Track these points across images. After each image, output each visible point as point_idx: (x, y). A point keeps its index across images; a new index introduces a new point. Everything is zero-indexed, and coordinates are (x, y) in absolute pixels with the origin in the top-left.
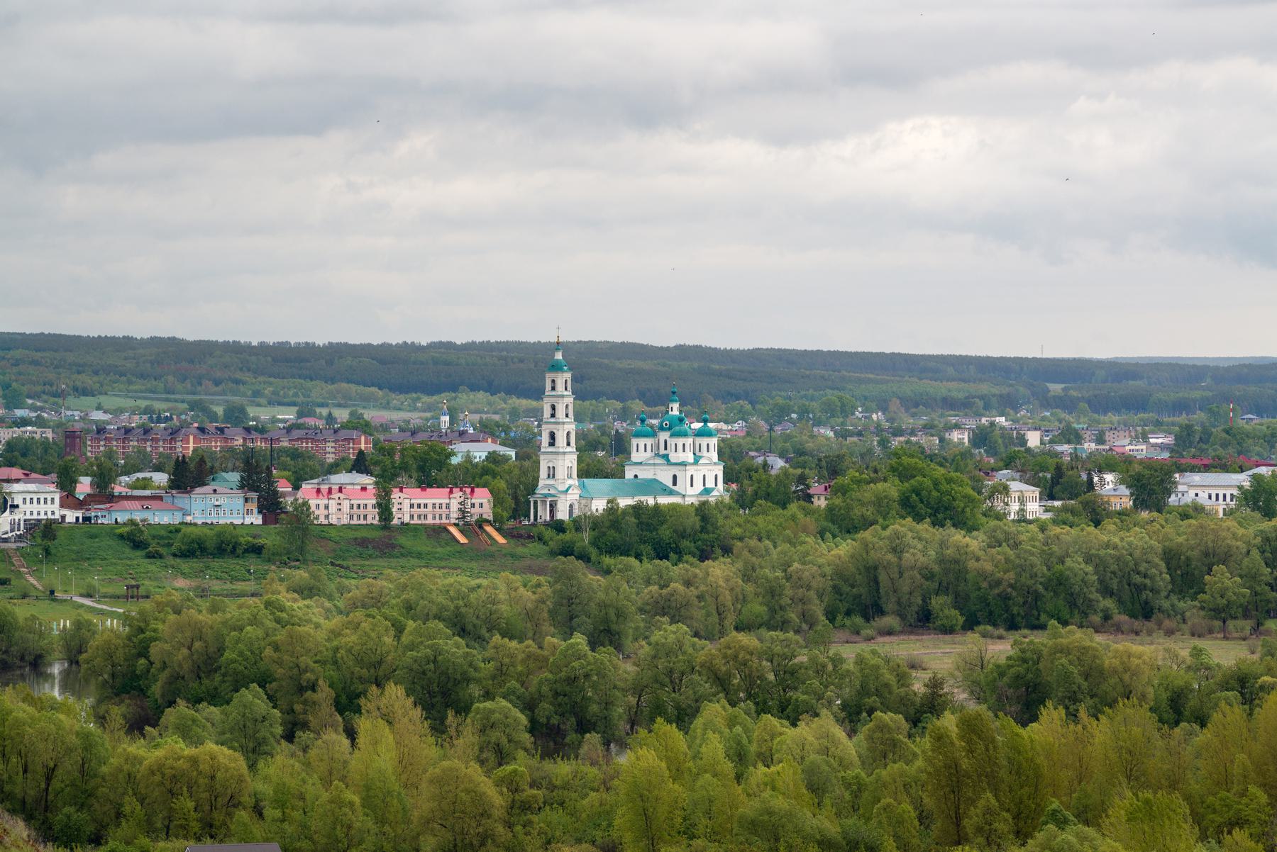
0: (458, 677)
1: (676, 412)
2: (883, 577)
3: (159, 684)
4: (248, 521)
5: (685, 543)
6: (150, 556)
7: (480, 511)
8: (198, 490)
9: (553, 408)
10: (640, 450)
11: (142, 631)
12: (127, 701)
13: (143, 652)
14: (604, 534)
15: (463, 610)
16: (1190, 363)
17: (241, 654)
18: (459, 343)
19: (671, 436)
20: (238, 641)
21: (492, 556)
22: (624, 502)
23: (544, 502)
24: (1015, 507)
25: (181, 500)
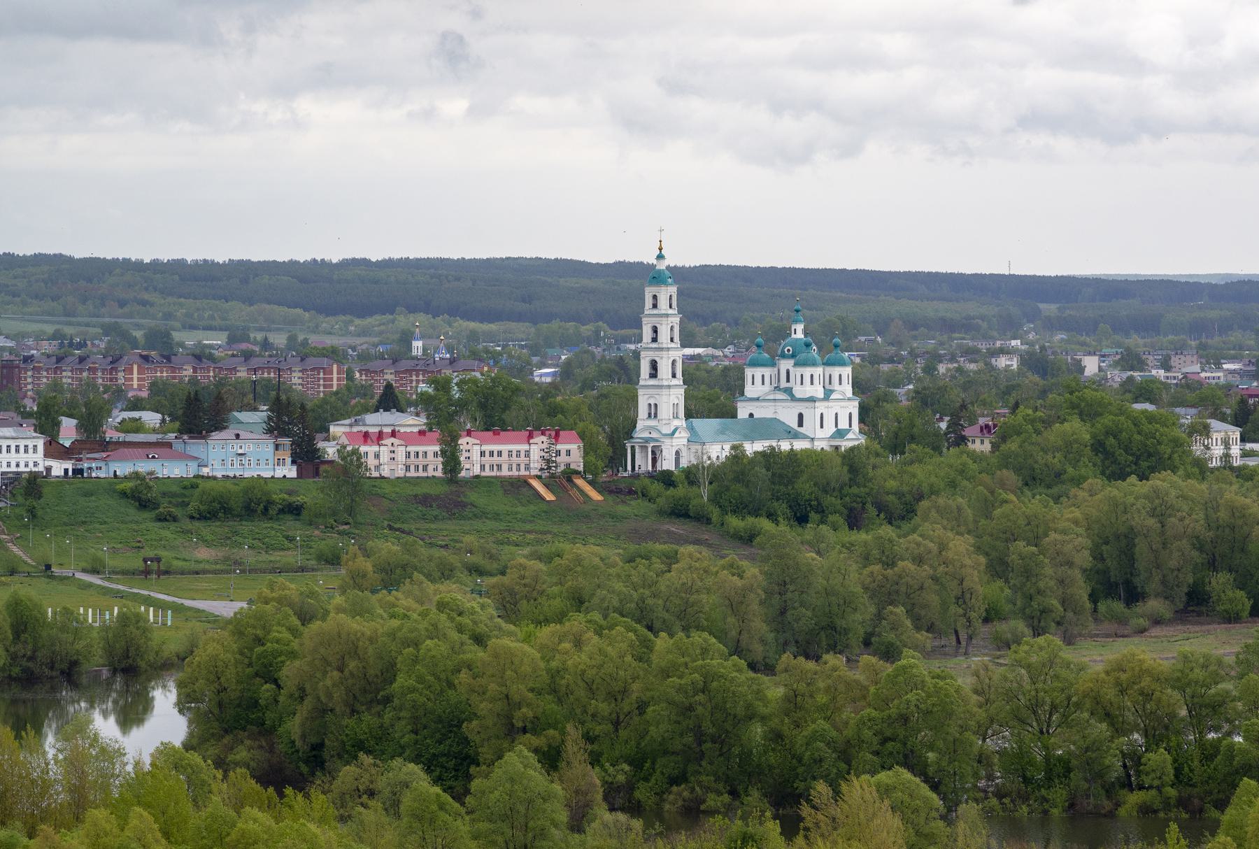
0: (740, 710)
1: (800, 335)
2: (1141, 548)
3: (298, 719)
4: (279, 473)
5: (830, 500)
6: (161, 519)
7: (567, 459)
8: (216, 435)
9: (655, 330)
10: (757, 382)
11: (259, 641)
12: (248, 742)
13: (268, 673)
14: (728, 489)
15: (650, 601)
16: (1183, 280)
17: (421, 679)
18: (374, 260)
19: (796, 365)
20: (416, 660)
21: (587, 517)
22: (751, 448)
23: (644, 448)
24: (1218, 451)
25: (195, 447)
